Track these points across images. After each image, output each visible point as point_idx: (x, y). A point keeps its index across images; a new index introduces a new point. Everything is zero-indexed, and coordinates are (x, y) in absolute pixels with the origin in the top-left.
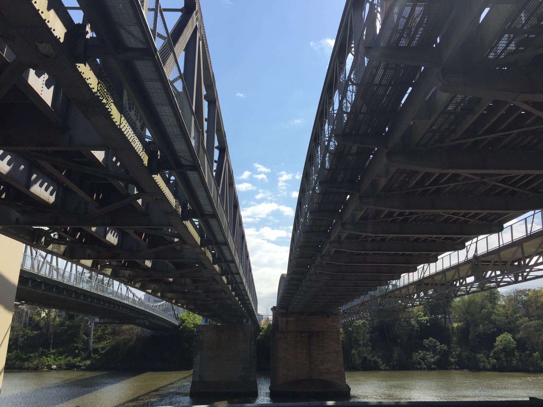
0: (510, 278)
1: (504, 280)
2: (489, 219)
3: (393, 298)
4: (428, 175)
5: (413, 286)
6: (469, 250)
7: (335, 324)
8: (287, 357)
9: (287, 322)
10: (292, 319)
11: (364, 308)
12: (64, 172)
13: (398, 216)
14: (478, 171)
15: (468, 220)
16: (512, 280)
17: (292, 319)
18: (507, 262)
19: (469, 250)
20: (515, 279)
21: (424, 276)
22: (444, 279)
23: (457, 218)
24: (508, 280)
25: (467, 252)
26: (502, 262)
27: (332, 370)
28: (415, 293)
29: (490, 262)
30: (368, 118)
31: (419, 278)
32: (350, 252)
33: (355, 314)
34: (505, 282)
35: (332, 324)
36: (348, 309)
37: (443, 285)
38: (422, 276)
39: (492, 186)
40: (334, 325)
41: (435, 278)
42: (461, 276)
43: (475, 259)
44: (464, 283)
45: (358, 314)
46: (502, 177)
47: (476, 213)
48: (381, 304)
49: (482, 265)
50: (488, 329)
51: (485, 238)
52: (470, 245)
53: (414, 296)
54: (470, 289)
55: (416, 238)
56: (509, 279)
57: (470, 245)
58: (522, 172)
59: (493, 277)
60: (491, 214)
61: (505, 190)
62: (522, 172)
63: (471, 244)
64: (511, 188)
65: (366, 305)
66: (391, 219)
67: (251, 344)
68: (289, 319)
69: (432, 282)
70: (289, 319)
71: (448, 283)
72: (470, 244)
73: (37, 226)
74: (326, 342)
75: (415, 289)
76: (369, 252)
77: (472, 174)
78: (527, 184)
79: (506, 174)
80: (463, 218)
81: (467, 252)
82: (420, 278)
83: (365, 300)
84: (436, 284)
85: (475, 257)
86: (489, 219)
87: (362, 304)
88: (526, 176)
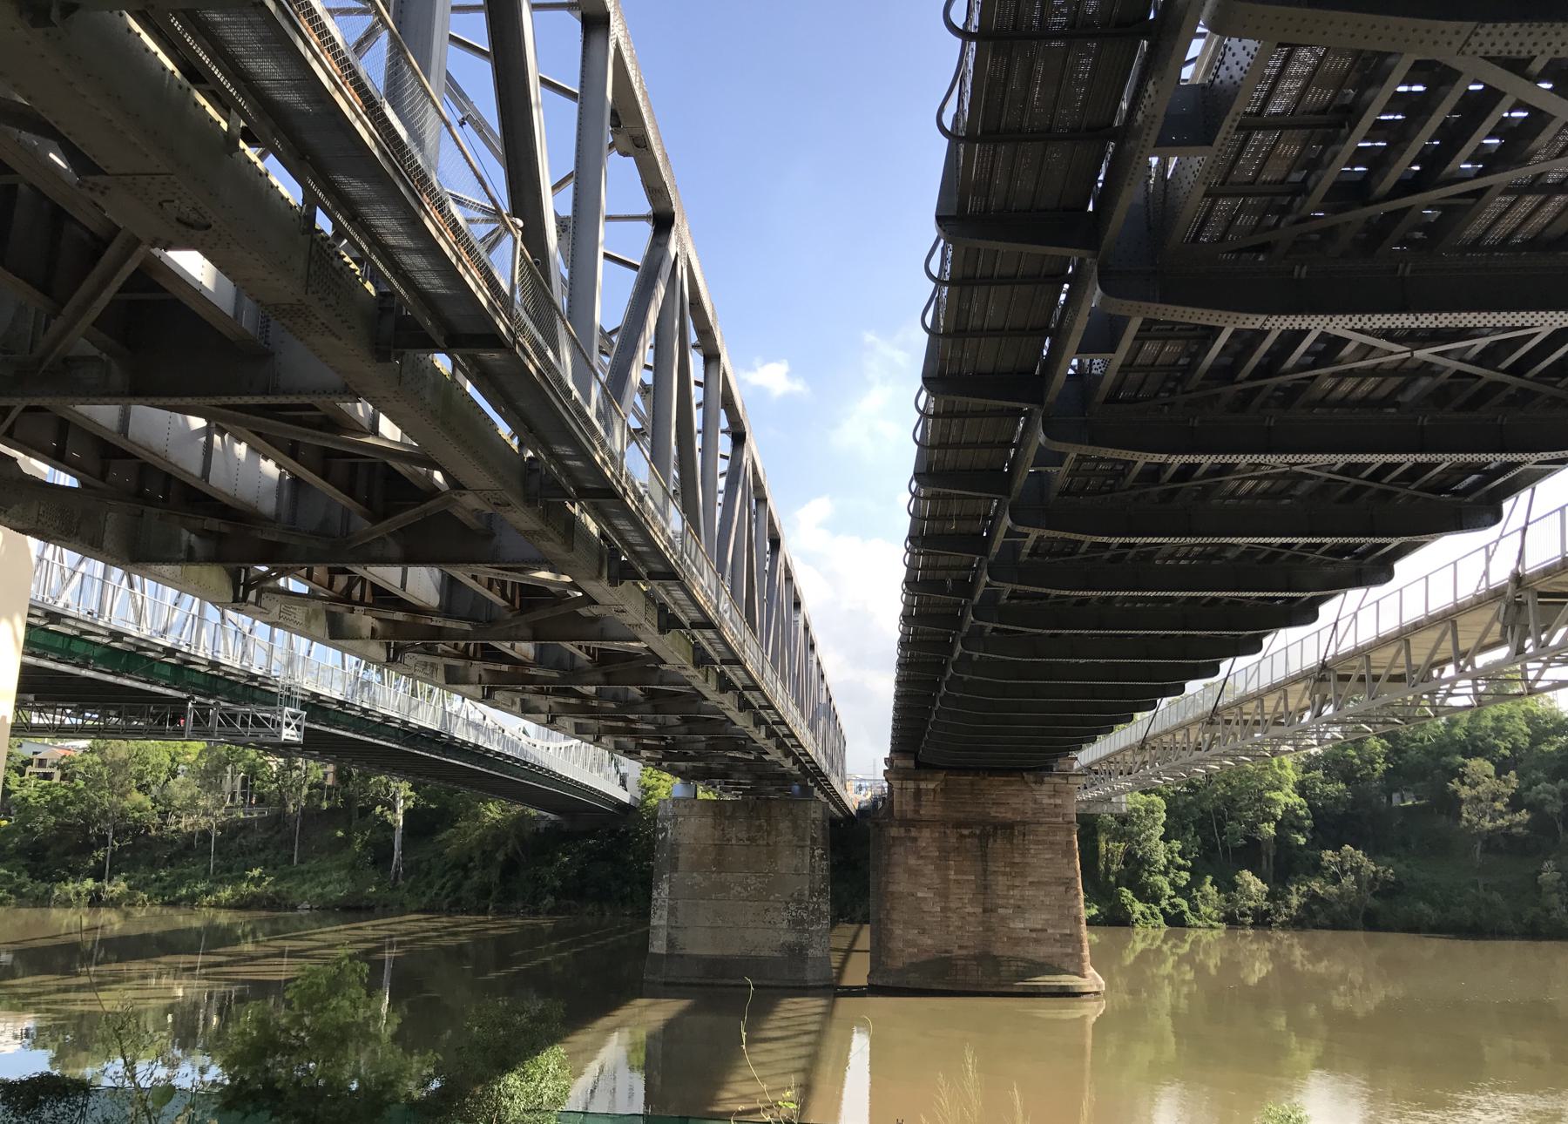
3: (1237, 723)
6: (1493, 552)
7: (1059, 801)
9: (918, 793)
10: (931, 786)
11: (1147, 758)
14: (1480, 317)
15: (1392, 491)
17: (931, 786)
19: (1493, 552)
21: (1336, 652)
22: (1402, 660)
28: (1307, 708)
30: (96, 716)
31: (1321, 658)
33: (1121, 774)
35: (1052, 801)
36: (1101, 759)
38: (1331, 652)
40: (1055, 805)
41: (1372, 656)
42: (1462, 647)
43: (1514, 586)
44: (1469, 669)
45: (1129, 774)
47: (1417, 465)
48: (1200, 744)
49: (1540, 603)
50: (992, 911)
51: (1554, 512)
52: (1497, 542)
54: (1443, 700)
55: (1244, 552)
57: (1497, 542)
63: (1502, 537)
65: (1153, 748)
67: (813, 856)
68: (923, 785)
69: (1364, 672)
70: (923, 785)
71: (1415, 672)
72: (1497, 537)
74: (1032, 851)
76: (1357, 540)
80: (1376, 485)
82: (1325, 657)
83: (1151, 732)
85: (1518, 579)
87: (1143, 744)
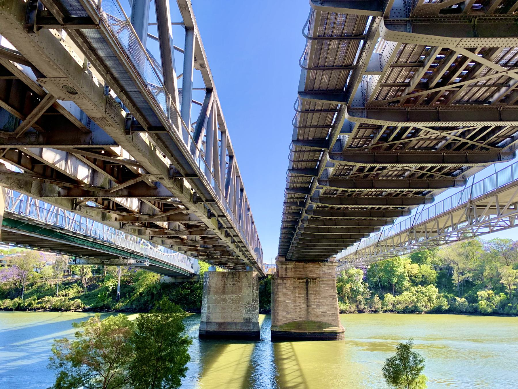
0: (504, 221)
1: (499, 223)
2: (454, 173)
4: (392, 130)
5: (405, 234)
7: (330, 271)
8: (287, 301)
9: (286, 269)
10: (291, 266)
12: (348, 83)
13: (368, 171)
16: (507, 224)
17: (291, 266)
18: (504, 206)
20: (510, 223)
22: (436, 226)
23: (424, 173)
24: (503, 223)
25: (461, 198)
26: (500, 206)
27: (328, 312)
29: (486, 206)
31: (411, 225)
32: (331, 207)
34: (500, 226)
35: (328, 271)
36: (343, 258)
37: (435, 232)
39: (452, 141)
46: (461, 131)
53: (405, 244)
56: (503, 222)
57: (464, 190)
58: (479, 125)
59: (487, 221)
60: (456, 169)
61: (465, 144)
62: (479, 125)
64: (471, 142)
66: (363, 174)
67: (253, 289)
68: (288, 266)
70: (288, 266)
71: (440, 230)
73: (211, 150)
75: (407, 237)
77: (429, 128)
78: (484, 139)
79: (467, 127)
81: (461, 198)
84: (428, 232)
86: (454, 173)
88: (485, 128)
